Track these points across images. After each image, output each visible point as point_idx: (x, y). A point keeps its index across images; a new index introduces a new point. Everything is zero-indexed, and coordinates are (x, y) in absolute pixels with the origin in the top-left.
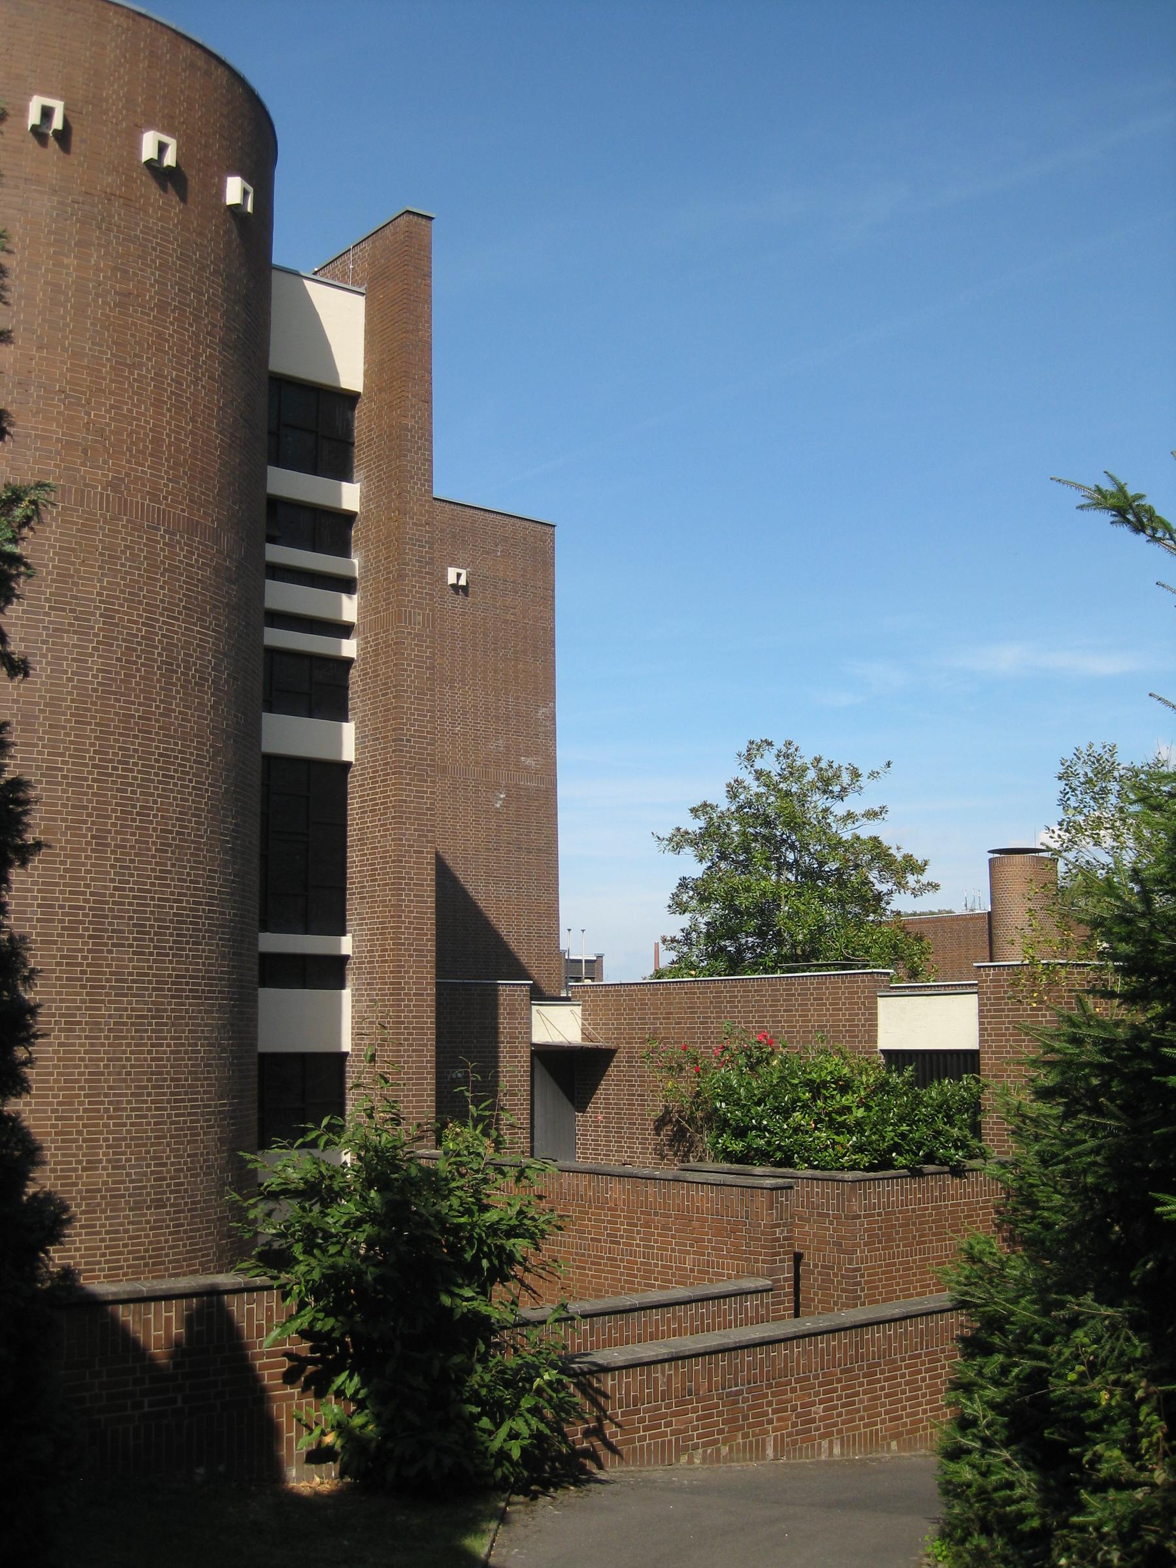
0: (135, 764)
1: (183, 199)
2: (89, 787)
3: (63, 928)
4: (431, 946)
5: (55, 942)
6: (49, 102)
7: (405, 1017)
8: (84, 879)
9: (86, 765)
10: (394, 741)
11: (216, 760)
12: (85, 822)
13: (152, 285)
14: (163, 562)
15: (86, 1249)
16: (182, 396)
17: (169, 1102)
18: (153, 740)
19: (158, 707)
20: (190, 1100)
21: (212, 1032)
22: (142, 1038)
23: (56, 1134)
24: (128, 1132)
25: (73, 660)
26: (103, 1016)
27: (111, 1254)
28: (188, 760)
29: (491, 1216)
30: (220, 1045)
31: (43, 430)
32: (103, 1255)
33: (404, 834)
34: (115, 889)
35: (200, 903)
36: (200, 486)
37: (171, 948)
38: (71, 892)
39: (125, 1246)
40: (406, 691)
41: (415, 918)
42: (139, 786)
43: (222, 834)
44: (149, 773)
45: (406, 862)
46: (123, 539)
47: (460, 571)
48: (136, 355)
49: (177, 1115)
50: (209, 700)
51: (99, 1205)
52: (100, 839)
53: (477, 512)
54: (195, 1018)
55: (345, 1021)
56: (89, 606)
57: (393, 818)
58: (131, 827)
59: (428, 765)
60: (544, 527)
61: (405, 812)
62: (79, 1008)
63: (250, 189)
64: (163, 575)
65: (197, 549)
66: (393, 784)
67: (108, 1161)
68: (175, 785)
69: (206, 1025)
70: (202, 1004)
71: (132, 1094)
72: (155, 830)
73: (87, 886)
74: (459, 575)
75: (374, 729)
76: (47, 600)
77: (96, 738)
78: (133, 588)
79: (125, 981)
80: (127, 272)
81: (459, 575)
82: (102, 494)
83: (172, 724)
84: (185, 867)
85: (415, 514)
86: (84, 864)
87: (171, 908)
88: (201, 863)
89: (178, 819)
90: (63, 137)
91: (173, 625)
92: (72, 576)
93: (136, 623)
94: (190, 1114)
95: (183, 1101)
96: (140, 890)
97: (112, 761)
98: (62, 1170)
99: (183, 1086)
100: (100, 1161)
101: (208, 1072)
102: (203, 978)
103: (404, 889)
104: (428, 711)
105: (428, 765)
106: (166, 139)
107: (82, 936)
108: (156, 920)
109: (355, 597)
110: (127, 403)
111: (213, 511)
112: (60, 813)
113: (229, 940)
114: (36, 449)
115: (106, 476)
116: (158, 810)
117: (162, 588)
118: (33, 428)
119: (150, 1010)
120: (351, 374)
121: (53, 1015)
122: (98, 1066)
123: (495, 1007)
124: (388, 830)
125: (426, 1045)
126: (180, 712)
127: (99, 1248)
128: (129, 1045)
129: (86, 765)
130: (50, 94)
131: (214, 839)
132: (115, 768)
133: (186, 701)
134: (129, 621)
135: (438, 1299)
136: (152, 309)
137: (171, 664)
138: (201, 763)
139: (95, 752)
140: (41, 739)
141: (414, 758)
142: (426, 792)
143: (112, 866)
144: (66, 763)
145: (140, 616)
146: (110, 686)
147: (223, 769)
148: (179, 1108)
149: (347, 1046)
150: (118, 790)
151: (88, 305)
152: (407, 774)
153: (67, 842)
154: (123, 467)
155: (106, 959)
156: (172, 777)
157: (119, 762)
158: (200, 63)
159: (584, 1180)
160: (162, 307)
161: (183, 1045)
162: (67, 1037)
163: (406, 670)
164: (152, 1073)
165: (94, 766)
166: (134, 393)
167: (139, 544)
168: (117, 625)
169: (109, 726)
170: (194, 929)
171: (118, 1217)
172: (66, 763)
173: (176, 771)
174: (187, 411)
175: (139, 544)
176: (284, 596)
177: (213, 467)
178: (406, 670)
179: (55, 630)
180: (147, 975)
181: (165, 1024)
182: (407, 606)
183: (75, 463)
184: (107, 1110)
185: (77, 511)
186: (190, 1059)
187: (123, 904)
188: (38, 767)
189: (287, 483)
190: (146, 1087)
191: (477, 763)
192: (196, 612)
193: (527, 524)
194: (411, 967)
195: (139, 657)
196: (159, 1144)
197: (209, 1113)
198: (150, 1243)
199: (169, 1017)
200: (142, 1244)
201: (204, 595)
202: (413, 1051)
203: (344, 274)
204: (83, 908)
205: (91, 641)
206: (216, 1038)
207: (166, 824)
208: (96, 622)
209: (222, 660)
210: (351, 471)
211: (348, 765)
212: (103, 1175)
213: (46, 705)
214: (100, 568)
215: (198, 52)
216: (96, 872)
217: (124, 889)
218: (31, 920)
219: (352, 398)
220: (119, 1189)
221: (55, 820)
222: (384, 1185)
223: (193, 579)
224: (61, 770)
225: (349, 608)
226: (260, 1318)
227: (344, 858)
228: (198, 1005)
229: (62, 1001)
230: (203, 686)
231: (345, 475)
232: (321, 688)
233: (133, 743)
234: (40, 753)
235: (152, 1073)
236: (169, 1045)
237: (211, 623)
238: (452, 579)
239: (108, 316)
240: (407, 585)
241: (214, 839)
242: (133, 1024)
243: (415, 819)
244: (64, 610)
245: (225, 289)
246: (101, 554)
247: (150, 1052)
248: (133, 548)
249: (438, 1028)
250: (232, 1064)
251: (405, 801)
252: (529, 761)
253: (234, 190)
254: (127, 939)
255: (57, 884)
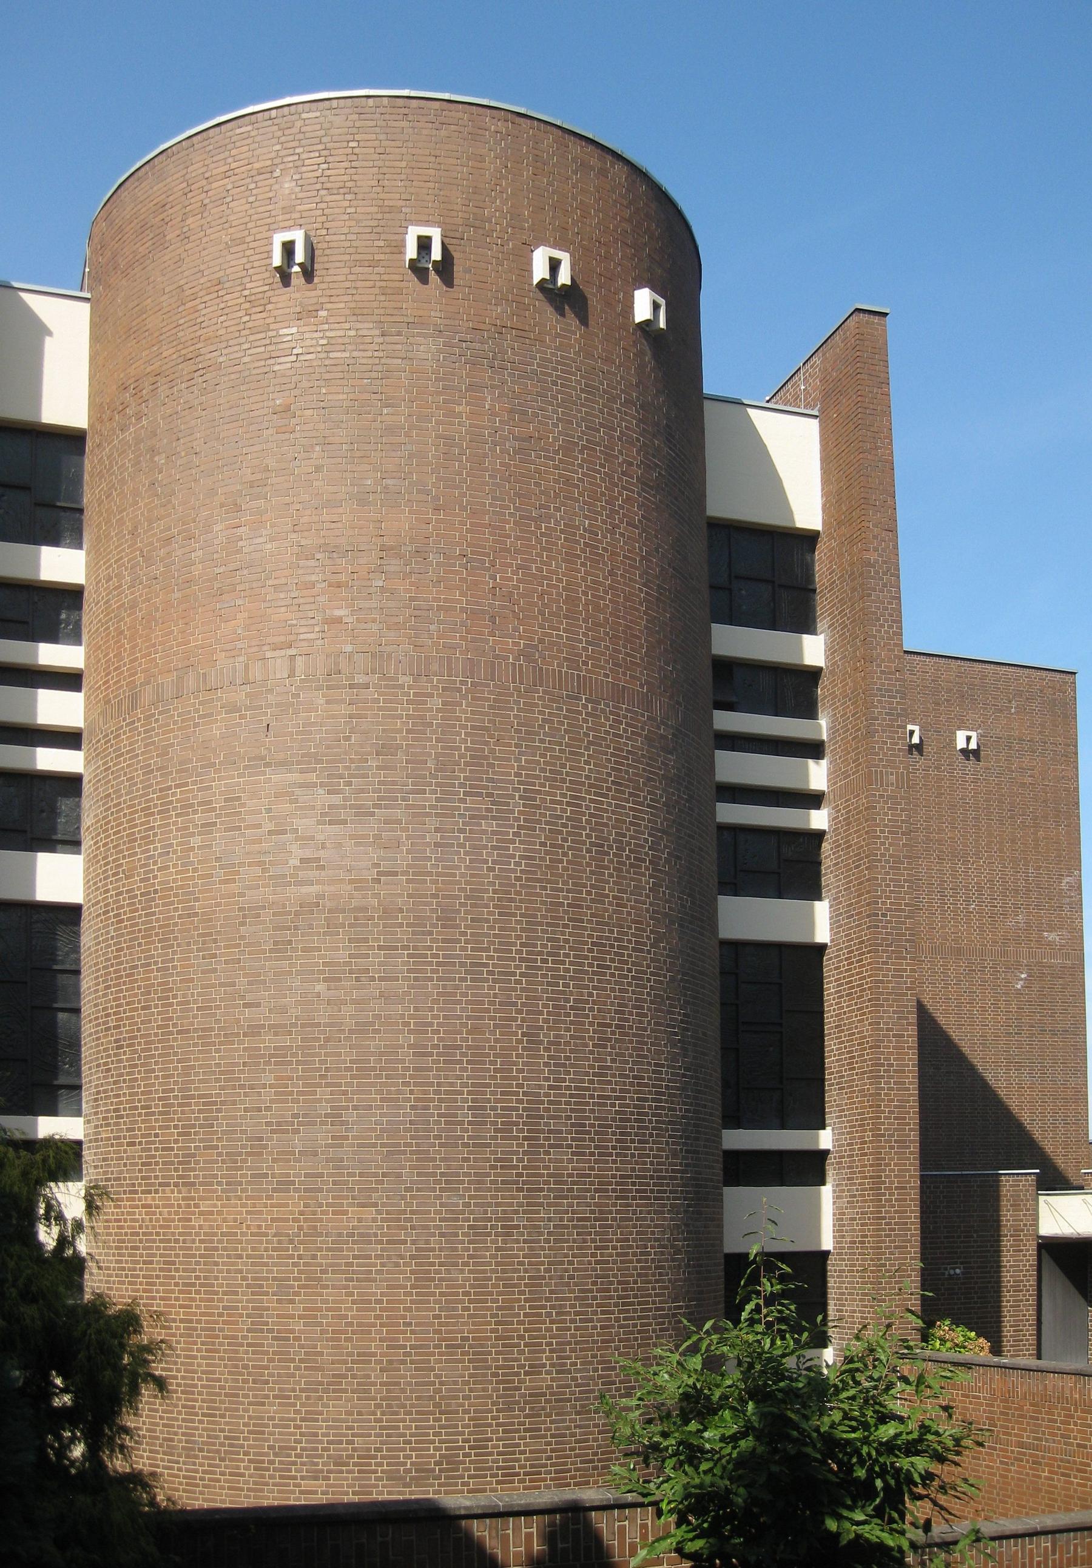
0: (567, 955)
1: (584, 321)
2: (518, 982)
3: (496, 1130)
4: (914, 1136)
5: (489, 1145)
6: (425, 231)
7: (886, 1212)
8: (516, 1078)
9: (513, 959)
10: (868, 916)
11: (658, 947)
12: (515, 1019)
13: (556, 425)
14: (587, 735)
15: (531, 1452)
16: (597, 548)
17: (616, 1305)
18: (585, 929)
19: (589, 893)
20: (639, 1303)
21: (663, 1233)
22: (585, 1241)
23: (497, 1338)
24: (573, 1336)
25: (494, 848)
26: (542, 1219)
27: (557, 1457)
28: (626, 948)
29: (888, 1431)
30: (673, 1246)
31: (446, 600)
32: (550, 1458)
33: (882, 1018)
34: (550, 1087)
35: (646, 1100)
36: (625, 647)
37: (614, 1148)
38: (502, 1093)
39: (572, 1449)
40: (880, 861)
41: (896, 1107)
42: (572, 978)
43: (668, 1026)
44: (582, 964)
45: (885, 1047)
46: (541, 713)
47: (969, 733)
48: (541, 506)
49: (625, 1319)
50: (647, 882)
51: (544, 1408)
52: (532, 1038)
53: (987, 666)
54: (645, 1219)
55: (826, 1217)
56: (507, 789)
57: (870, 1000)
58: (565, 1022)
59: (907, 941)
60: (1063, 676)
61: (882, 993)
62: (516, 1212)
63: (662, 301)
64: (587, 749)
65: (626, 717)
66: (869, 964)
67: (552, 1365)
68: (612, 975)
69: (656, 1226)
70: (651, 1205)
71: (576, 1298)
72: (591, 1024)
73: (521, 1086)
74: (969, 739)
75: (849, 905)
76: (462, 785)
77: (522, 930)
78: (555, 765)
79: (565, 1183)
80: (525, 413)
81: (969, 739)
82: (514, 665)
83: (607, 910)
84: (627, 1062)
85: (883, 661)
86: (515, 1064)
87: (613, 1105)
88: (645, 1057)
89: (616, 1012)
90: (445, 268)
91: (602, 803)
92: (486, 758)
93: (560, 803)
94: (639, 1318)
95: (633, 1304)
96: (576, 1088)
97: (540, 953)
98: (503, 1375)
99: (632, 1289)
100: (544, 1365)
101: (660, 1274)
102: (652, 1177)
103: (883, 1077)
104: (905, 881)
105: (907, 941)
106: (557, 254)
107: (517, 1138)
108: (596, 1119)
109: (824, 763)
110: (535, 562)
111: (641, 673)
112: (488, 1011)
113: (681, 1137)
114: (440, 622)
115: (517, 644)
116: (594, 1003)
117: (587, 763)
118: (435, 600)
119: (592, 1212)
120: (807, 510)
121: (490, 1220)
122: (539, 1270)
123: (997, 1198)
124: (864, 1014)
125: (910, 1241)
126: (614, 897)
127: (545, 1451)
128: (571, 1248)
129: (513, 959)
130: (427, 223)
131: (660, 1031)
132: (545, 961)
133: (621, 884)
134: (552, 802)
135: (823, 1522)
136: (557, 452)
137: (602, 846)
138: (642, 951)
139: (522, 945)
140: (464, 934)
141: (891, 934)
142: (905, 970)
143: (546, 1064)
144: (491, 958)
145: (564, 795)
146: (535, 873)
147: (668, 956)
148: (628, 1311)
149: (827, 1243)
150: (549, 984)
151: (485, 456)
152: (883, 951)
153: (496, 1041)
154: (536, 633)
155: (543, 1160)
156: (609, 967)
157: (549, 954)
158: (594, 162)
159: (1070, 1382)
160: (568, 449)
161: (631, 1247)
162: (504, 1242)
163: (879, 837)
164: (597, 1276)
165: (521, 960)
166: (543, 549)
167: (559, 716)
168: (538, 807)
169: (536, 916)
170: (639, 1128)
171: (564, 1421)
172: (491, 958)
173: (612, 960)
174: (605, 564)
175: (559, 716)
176: (734, 767)
177: (638, 624)
178: (879, 837)
179: (472, 817)
180: (589, 1176)
181: (611, 1226)
182: (877, 766)
183: (482, 633)
184: (549, 1315)
185: (488, 686)
186: (638, 1261)
187: (560, 1103)
188: (462, 964)
189: (738, 641)
190: (592, 1291)
191: (995, 942)
192: (627, 787)
193: (1044, 674)
194: (892, 1159)
195: (565, 840)
196: (607, 1348)
197: (661, 1316)
198: (599, 1447)
199: (614, 1219)
200: (591, 1447)
201: (637, 768)
202: (896, 1247)
203: (797, 398)
204: (517, 1109)
205: (512, 827)
206: (669, 1239)
207: (604, 1018)
208: (516, 805)
209: (661, 838)
210: (814, 622)
211: (822, 948)
212: (546, 1379)
213: (467, 897)
214: (517, 746)
215: (590, 148)
216: (529, 1071)
217: (560, 1088)
218: (462, 1123)
219: (810, 538)
220: (565, 1393)
221: (482, 1018)
222: (757, 1394)
223: (622, 750)
224: (486, 965)
225: (818, 775)
226: (633, 1535)
227: (822, 1047)
228: (646, 1205)
229: (498, 1205)
230: (640, 867)
231: (807, 626)
232: (793, 867)
233: (563, 933)
234: (463, 949)
235: (597, 1276)
236: (614, 1248)
237: (645, 798)
238: (961, 744)
239: (508, 466)
240: (877, 742)
241: (660, 1031)
242: (574, 1227)
243: (894, 1000)
244: (480, 795)
245: (640, 421)
246: (517, 731)
247: (593, 1255)
248: (551, 722)
249: (922, 1223)
250: (688, 1266)
251: (882, 982)
252: (1052, 936)
253: (644, 304)
254: (566, 1139)
255: (488, 1085)
